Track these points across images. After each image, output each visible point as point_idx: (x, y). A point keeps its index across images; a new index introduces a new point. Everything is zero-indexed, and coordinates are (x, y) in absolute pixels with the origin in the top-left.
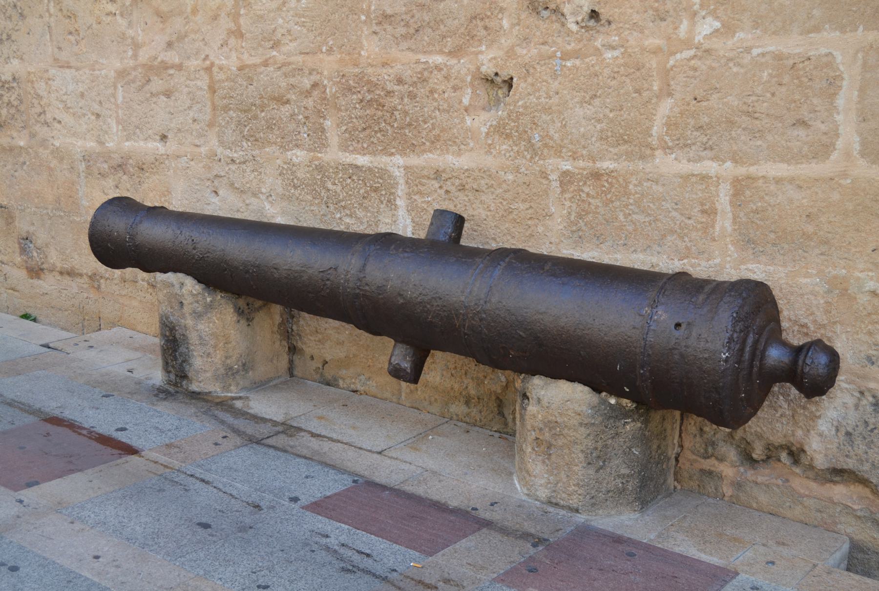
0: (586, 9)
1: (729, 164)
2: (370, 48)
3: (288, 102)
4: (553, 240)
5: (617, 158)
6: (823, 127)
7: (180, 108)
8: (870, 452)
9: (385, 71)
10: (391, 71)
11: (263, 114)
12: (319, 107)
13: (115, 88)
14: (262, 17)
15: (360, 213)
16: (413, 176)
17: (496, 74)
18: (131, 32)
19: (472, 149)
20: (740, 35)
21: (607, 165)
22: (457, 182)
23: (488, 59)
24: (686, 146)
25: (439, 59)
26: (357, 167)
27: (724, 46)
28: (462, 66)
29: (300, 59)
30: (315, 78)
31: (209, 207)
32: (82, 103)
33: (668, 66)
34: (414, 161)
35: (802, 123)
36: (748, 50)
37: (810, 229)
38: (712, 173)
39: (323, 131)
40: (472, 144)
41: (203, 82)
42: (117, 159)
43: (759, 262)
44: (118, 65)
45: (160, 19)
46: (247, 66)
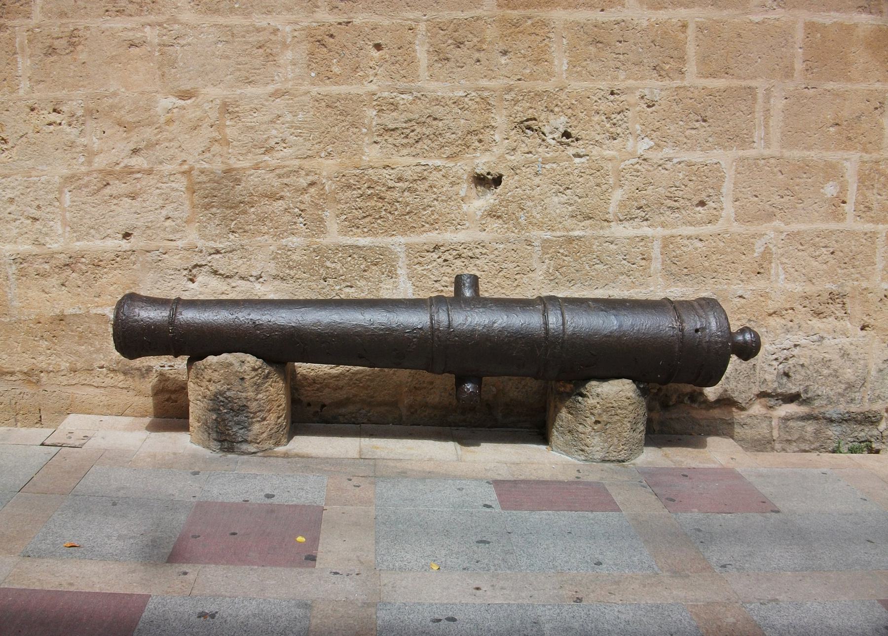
0: (562, 130)
1: (659, 229)
2: (372, 154)
3: (282, 198)
4: (535, 287)
5: (584, 228)
6: (714, 205)
7: (150, 208)
8: (739, 386)
9: (386, 172)
10: (392, 171)
11: (253, 210)
12: (316, 201)
13: (61, 192)
14: (252, 128)
15: (362, 283)
16: (417, 254)
17: (489, 174)
18: (83, 140)
20: (666, 150)
21: (576, 233)
22: (455, 253)
23: (483, 163)
24: (631, 219)
25: (438, 162)
26: (358, 247)
27: (656, 156)
29: (297, 162)
30: (310, 178)
31: (186, 293)
32: (13, 208)
33: (620, 168)
34: (415, 239)
35: (702, 204)
36: (670, 160)
37: (707, 264)
38: (649, 235)
39: (322, 220)
40: (467, 225)
41: (181, 184)
42: (63, 259)
43: (677, 286)
44: (66, 172)
45: (122, 129)
46: (234, 169)
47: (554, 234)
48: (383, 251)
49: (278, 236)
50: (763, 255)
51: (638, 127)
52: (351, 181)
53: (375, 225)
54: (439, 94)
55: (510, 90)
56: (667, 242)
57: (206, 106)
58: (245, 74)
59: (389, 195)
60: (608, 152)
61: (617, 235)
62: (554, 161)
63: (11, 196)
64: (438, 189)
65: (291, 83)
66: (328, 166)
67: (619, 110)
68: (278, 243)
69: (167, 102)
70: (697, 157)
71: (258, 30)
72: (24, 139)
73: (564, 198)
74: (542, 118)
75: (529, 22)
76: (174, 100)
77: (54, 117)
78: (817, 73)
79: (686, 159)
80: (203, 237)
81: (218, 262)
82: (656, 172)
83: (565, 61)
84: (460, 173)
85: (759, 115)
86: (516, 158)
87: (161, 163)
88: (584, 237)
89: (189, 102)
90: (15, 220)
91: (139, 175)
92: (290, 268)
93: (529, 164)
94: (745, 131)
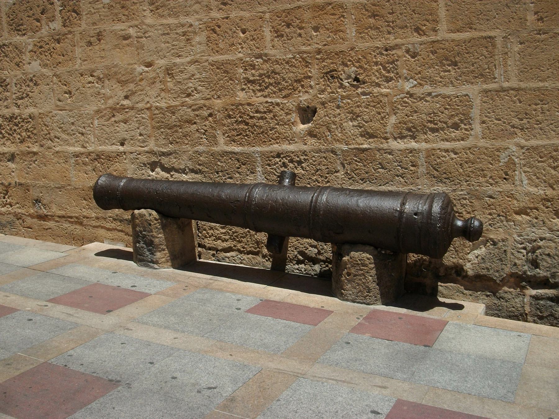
0: (353, 76)
3: (195, 123)
13: (93, 119)
14: (180, 82)
16: (267, 158)
18: (103, 91)
19: (296, 142)
21: (365, 146)
23: (304, 98)
25: (278, 100)
26: (234, 153)
27: (419, 91)
28: (290, 104)
29: (202, 102)
32: (73, 128)
38: (416, 148)
39: (215, 137)
43: (439, 186)
46: (171, 106)
47: (350, 147)
48: (248, 156)
49: (193, 146)
50: (507, 164)
51: (405, 71)
52: (230, 113)
53: (244, 140)
54: (278, 57)
55: (319, 52)
56: (430, 153)
57: (158, 71)
58: (175, 51)
59: (250, 121)
60: (385, 90)
61: (393, 147)
62: (348, 97)
63: (73, 121)
64: (278, 117)
65: (199, 55)
66: (218, 103)
67: (391, 60)
68: (193, 149)
69: (141, 68)
70: (449, 91)
71: (183, 26)
72: (78, 91)
73: (355, 123)
74: (340, 69)
75: (330, 7)
76: (143, 68)
77: (91, 79)
78: (547, 21)
79: (442, 93)
80: (157, 145)
81: (165, 160)
82: (419, 103)
83: (354, 30)
84: (291, 107)
85: (499, 58)
86: (323, 97)
87: (137, 103)
88: (369, 149)
89: (150, 68)
90: (74, 134)
91: (127, 110)
92: (200, 165)
93: (333, 100)
94: (488, 70)
